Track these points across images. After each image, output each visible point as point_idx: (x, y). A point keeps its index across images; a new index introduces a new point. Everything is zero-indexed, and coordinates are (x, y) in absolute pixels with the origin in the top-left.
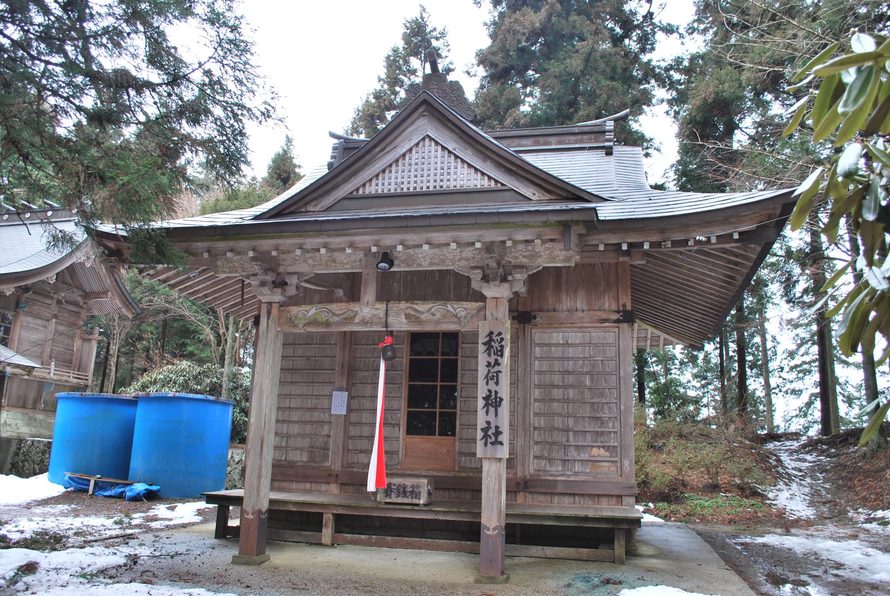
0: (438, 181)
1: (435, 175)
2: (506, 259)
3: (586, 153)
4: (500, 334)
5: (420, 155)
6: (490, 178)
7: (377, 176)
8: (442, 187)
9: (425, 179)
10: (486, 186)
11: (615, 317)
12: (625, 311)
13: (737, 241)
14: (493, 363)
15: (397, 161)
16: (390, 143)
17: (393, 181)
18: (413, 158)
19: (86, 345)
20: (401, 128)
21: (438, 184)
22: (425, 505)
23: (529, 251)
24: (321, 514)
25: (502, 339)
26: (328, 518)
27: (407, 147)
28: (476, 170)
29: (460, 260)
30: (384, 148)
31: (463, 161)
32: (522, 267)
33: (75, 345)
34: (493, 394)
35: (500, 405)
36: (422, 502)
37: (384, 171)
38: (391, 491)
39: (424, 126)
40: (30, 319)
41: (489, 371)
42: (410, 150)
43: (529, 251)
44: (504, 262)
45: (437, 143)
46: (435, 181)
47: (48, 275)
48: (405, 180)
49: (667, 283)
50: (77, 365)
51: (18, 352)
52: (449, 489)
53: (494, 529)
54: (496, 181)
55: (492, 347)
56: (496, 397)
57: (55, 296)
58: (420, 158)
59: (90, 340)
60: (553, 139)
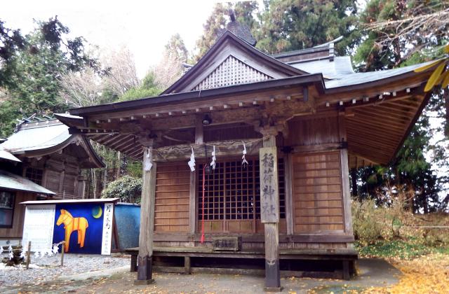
2: (273, 113)
4: (271, 154)
6: (265, 75)
7: (205, 79)
11: (337, 145)
12: (343, 142)
13: (409, 94)
15: (215, 70)
16: (211, 61)
17: (213, 82)
19: (80, 183)
20: (216, 53)
21: (237, 81)
24: (183, 258)
25: (272, 157)
26: (187, 260)
27: (221, 63)
28: (257, 71)
29: (247, 116)
31: (250, 67)
32: (282, 117)
36: (235, 249)
39: (229, 51)
42: (222, 64)
45: (236, 59)
53: (273, 262)
54: (268, 77)
60: (301, 56)
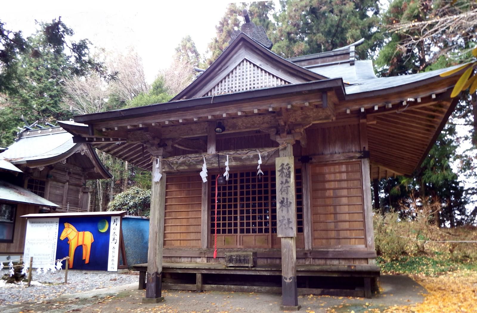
0: (252, 84)
1: (250, 81)
2: (290, 120)
3: (338, 66)
4: (288, 164)
5: (241, 71)
6: (281, 80)
7: (218, 85)
8: (254, 88)
9: (244, 84)
10: (279, 84)
11: (358, 155)
12: (364, 151)
13: (434, 100)
14: (284, 181)
15: (228, 75)
16: (224, 65)
17: (227, 87)
18: (238, 73)
19: (85, 195)
20: (230, 56)
21: (252, 86)
22: (252, 267)
23: (303, 114)
25: (289, 168)
27: (234, 67)
28: (273, 76)
29: (263, 123)
30: (221, 69)
31: (266, 72)
33: (79, 195)
34: (285, 200)
35: (290, 206)
37: (221, 82)
38: (232, 260)
39: (243, 54)
40: (55, 183)
41: (282, 187)
42: (236, 68)
43: (303, 114)
44: (289, 123)
45: (250, 63)
46: (250, 85)
47: (62, 160)
48: (234, 86)
49: (390, 136)
50: (81, 205)
51: (49, 200)
52: (267, 258)
53: (290, 279)
54: (285, 82)
55: (284, 172)
56: (287, 202)
57: (68, 171)
58: (241, 72)
59: (87, 193)
60: (319, 60)
